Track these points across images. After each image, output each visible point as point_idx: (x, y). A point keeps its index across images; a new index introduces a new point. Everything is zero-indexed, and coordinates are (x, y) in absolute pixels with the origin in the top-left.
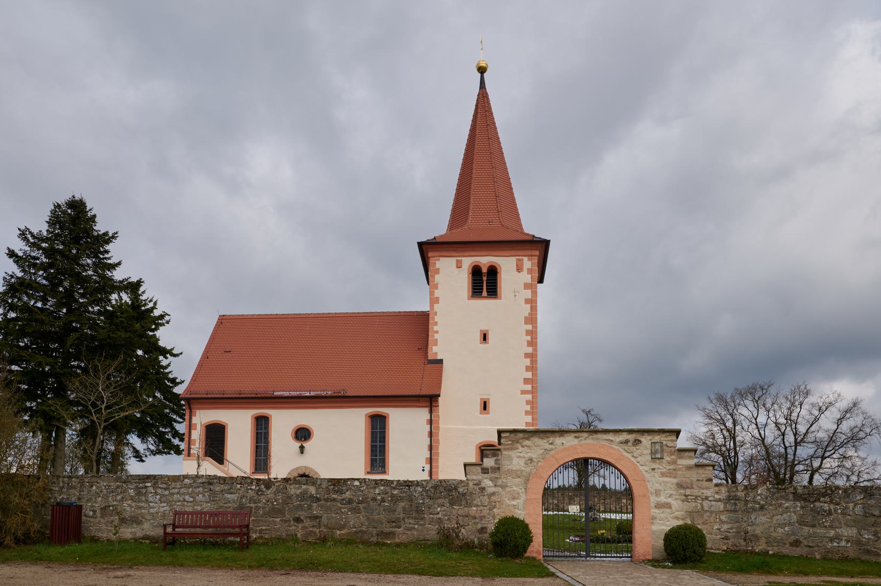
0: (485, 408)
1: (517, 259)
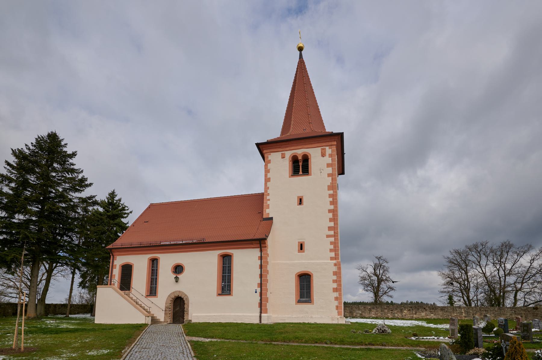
0: (301, 249)
1: (321, 149)
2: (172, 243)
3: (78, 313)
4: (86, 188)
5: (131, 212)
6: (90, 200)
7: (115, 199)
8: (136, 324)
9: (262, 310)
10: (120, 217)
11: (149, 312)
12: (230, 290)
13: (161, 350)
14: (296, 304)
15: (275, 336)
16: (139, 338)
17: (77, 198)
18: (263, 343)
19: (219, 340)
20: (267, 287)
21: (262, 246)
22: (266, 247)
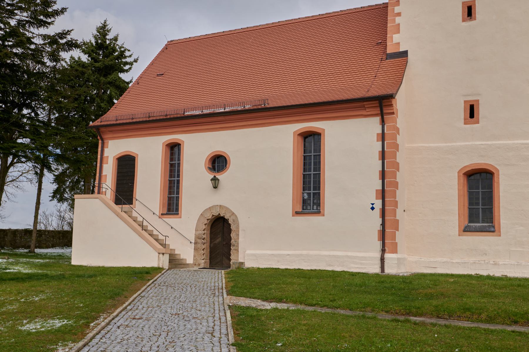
0: (472, 115)
2: (206, 111)
3: (53, 246)
4: (56, 17)
5: (136, 61)
6: (61, 38)
7: (107, 37)
8: (143, 267)
9: (386, 245)
10: (116, 70)
11: (164, 245)
12: (319, 205)
13: (169, 323)
14: (459, 235)
15: (417, 304)
16: (135, 296)
17: (41, 35)
18: (389, 317)
19: (292, 307)
20: (395, 197)
21: (385, 111)
22: (393, 113)
